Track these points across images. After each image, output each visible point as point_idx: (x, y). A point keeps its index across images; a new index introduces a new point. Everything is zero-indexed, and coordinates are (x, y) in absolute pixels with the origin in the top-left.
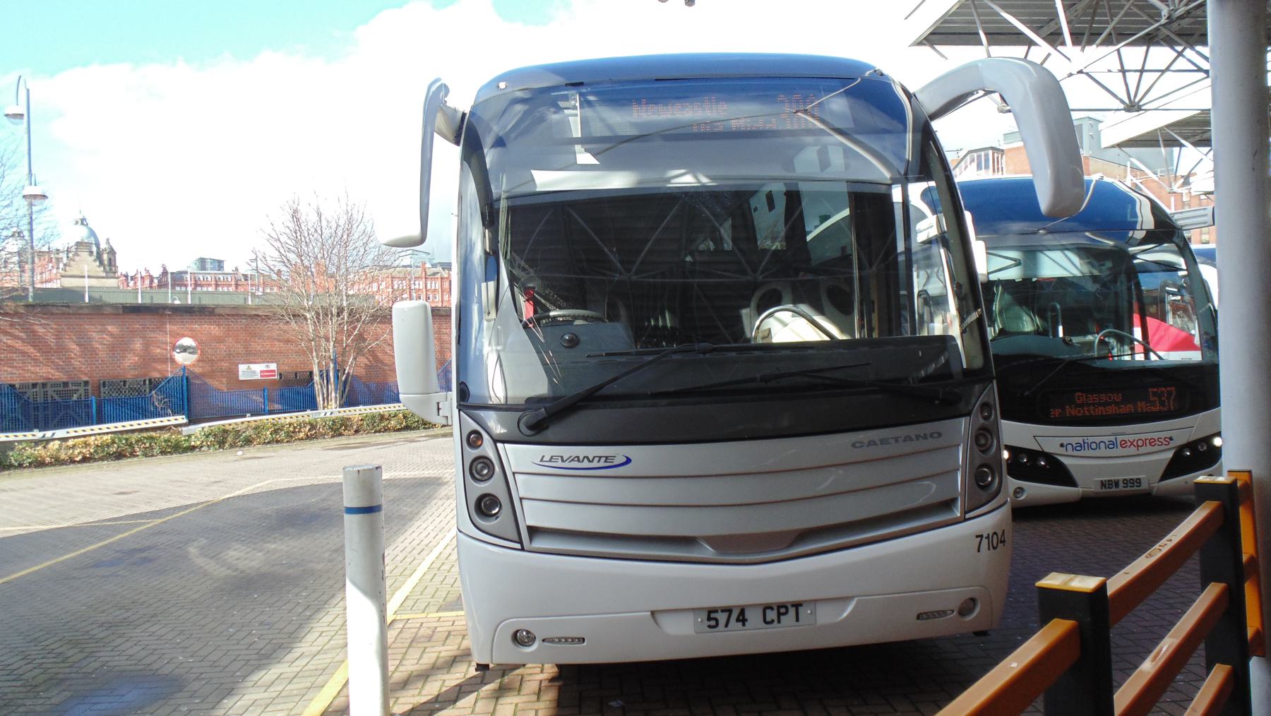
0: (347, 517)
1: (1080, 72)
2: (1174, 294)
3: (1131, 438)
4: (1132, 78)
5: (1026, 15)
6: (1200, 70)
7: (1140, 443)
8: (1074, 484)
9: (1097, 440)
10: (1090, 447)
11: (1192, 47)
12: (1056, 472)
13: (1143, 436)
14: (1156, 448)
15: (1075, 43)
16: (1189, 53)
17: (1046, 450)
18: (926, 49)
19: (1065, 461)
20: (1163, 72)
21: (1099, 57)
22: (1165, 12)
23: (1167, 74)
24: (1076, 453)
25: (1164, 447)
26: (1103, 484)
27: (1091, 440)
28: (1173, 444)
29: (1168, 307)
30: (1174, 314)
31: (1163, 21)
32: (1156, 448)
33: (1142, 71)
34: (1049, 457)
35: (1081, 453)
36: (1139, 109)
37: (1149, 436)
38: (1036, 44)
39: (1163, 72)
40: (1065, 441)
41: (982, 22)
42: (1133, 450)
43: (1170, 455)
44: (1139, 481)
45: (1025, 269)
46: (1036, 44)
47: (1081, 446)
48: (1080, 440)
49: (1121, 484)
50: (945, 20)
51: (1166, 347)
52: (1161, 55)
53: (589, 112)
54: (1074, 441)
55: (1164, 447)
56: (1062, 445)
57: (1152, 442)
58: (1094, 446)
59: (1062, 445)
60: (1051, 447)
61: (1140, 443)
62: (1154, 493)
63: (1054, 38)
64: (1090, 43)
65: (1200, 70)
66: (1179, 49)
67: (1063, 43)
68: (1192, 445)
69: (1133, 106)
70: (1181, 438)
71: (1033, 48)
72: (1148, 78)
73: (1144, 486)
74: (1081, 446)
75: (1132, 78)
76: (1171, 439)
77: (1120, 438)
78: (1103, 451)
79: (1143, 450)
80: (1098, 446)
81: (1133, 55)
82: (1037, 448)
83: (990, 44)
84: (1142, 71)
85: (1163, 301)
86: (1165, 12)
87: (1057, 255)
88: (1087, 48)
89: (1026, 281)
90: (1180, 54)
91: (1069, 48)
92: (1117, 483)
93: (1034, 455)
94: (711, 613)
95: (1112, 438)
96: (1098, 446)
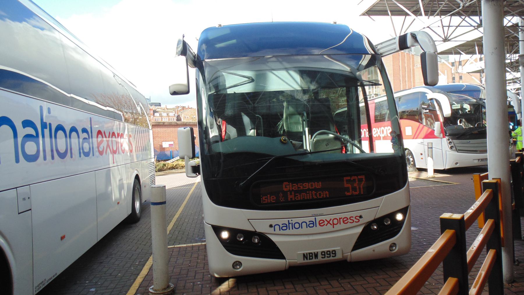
0: (152, 206)
1: (428, 27)
2: (426, 109)
3: (328, 218)
4: (446, 29)
5: (409, 7)
6: (471, 26)
7: (335, 222)
8: (280, 256)
9: (300, 220)
10: (294, 227)
11: (469, 16)
12: (266, 247)
13: (338, 216)
14: (349, 225)
15: (426, 15)
16: (467, 19)
17: (259, 230)
18: (367, 17)
19: (274, 239)
20: (459, 26)
21: (435, 20)
22: (462, 5)
23: (459, 27)
24: (282, 232)
25: (355, 224)
26: (305, 256)
27: (294, 221)
28: (362, 221)
29: (423, 116)
30: (426, 119)
31: (461, 8)
32: (349, 225)
33: (449, 26)
34: (262, 237)
35: (287, 232)
36: (449, 40)
37: (343, 216)
38: (408, 15)
39: (459, 26)
40: (273, 222)
41: (389, 7)
42: (329, 227)
43: (360, 230)
44: (334, 252)
45: (257, 85)
46: (408, 15)
47: (286, 226)
48: (286, 221)
49: (320, 256)
50: (374, 6)
51: (423, 137)
52: (456, 20)
53: (376, 79)
54: (280, 222)
55: (355, 224)
56: (271, 226)
57: (345, 220)
58: (297, 226)
59: (271, 226)
60: (262, 227)
61: (335, 222)
62: (348, 260)
63: (417, 12)
64: (432, 15)
65: (471, 26)
66: (463, 17)
67: (421, 15)
68: (379, 221)
69: (446, 40)
70: (369, 216)
71: (407, 17)
72: (451, 29)
73: (339, 256)
74: (286, 226)
75: (446, 29)
76: (361, 217)
77: (318, 218)
78: (305, 230)
79: (337, 227)
80: (301, 226)
81: (446, 19)
82: (251, 229)
83: (392, 15)
84: (449, 26)
85: (421, 114)
86: (462, 5)
87: (283, 74)
88: (431, 17)
89: (253, 96)
90: (464, 20)
91: (424, 18)
92: (316, 256)
93: (249, 234)
94: (479, 160)
95: (313, 219)
96: (301, 226)
